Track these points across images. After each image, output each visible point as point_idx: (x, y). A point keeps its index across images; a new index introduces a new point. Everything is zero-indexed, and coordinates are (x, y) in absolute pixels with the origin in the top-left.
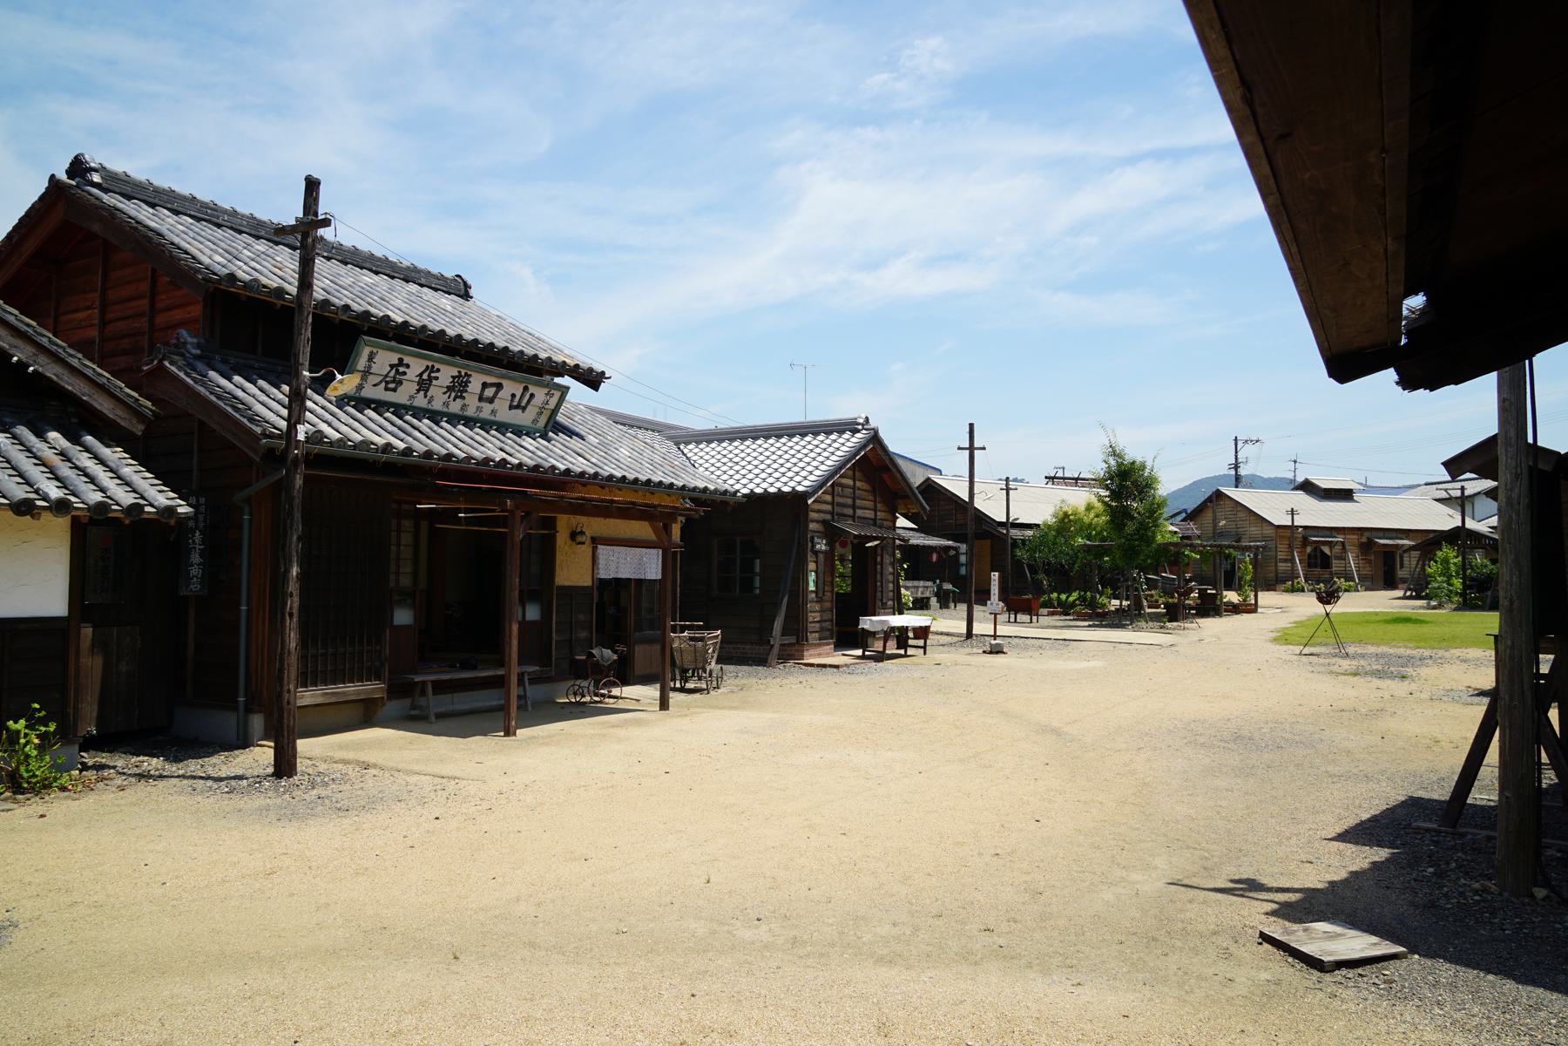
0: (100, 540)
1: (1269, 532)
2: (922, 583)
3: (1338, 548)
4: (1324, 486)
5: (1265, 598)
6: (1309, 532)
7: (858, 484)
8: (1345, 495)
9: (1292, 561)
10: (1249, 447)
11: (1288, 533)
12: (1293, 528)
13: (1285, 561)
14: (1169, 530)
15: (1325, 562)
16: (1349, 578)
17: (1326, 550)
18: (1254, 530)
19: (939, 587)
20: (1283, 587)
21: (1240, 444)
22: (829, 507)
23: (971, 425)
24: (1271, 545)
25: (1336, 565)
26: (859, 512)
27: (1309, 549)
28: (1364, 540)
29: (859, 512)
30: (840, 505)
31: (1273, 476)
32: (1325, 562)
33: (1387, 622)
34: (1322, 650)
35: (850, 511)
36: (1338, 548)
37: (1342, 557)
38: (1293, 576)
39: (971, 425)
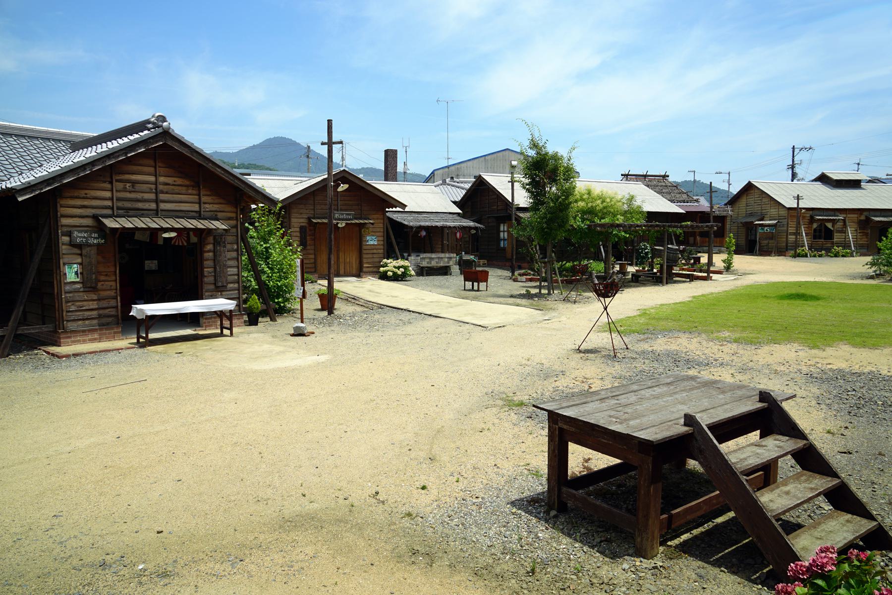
1: (783, 212)
2: (433, 256)
3: (839, 225)
4: (835, 177)
7: (162, 179)
8: (854, 184)
9: (800, 234)
12: (797, 209)
15: (829, 235)
16: (846, 245)
17: (829, 225)
18: (773, 211)
19: (461, 258)
21: (796, 151)
22: (109, 203)
24: (785, 222)
25: (837, 237)
26: (163, 206)
27: (815, 225)
28: (863, 218)
29: (163, 206)
30: (119, 199)
31: (261, 141)
32: (829, 235)
33: (783, 297)
35: (153, 206)
36: (839, 225)
37: (843, 231)
38: (797, 245)
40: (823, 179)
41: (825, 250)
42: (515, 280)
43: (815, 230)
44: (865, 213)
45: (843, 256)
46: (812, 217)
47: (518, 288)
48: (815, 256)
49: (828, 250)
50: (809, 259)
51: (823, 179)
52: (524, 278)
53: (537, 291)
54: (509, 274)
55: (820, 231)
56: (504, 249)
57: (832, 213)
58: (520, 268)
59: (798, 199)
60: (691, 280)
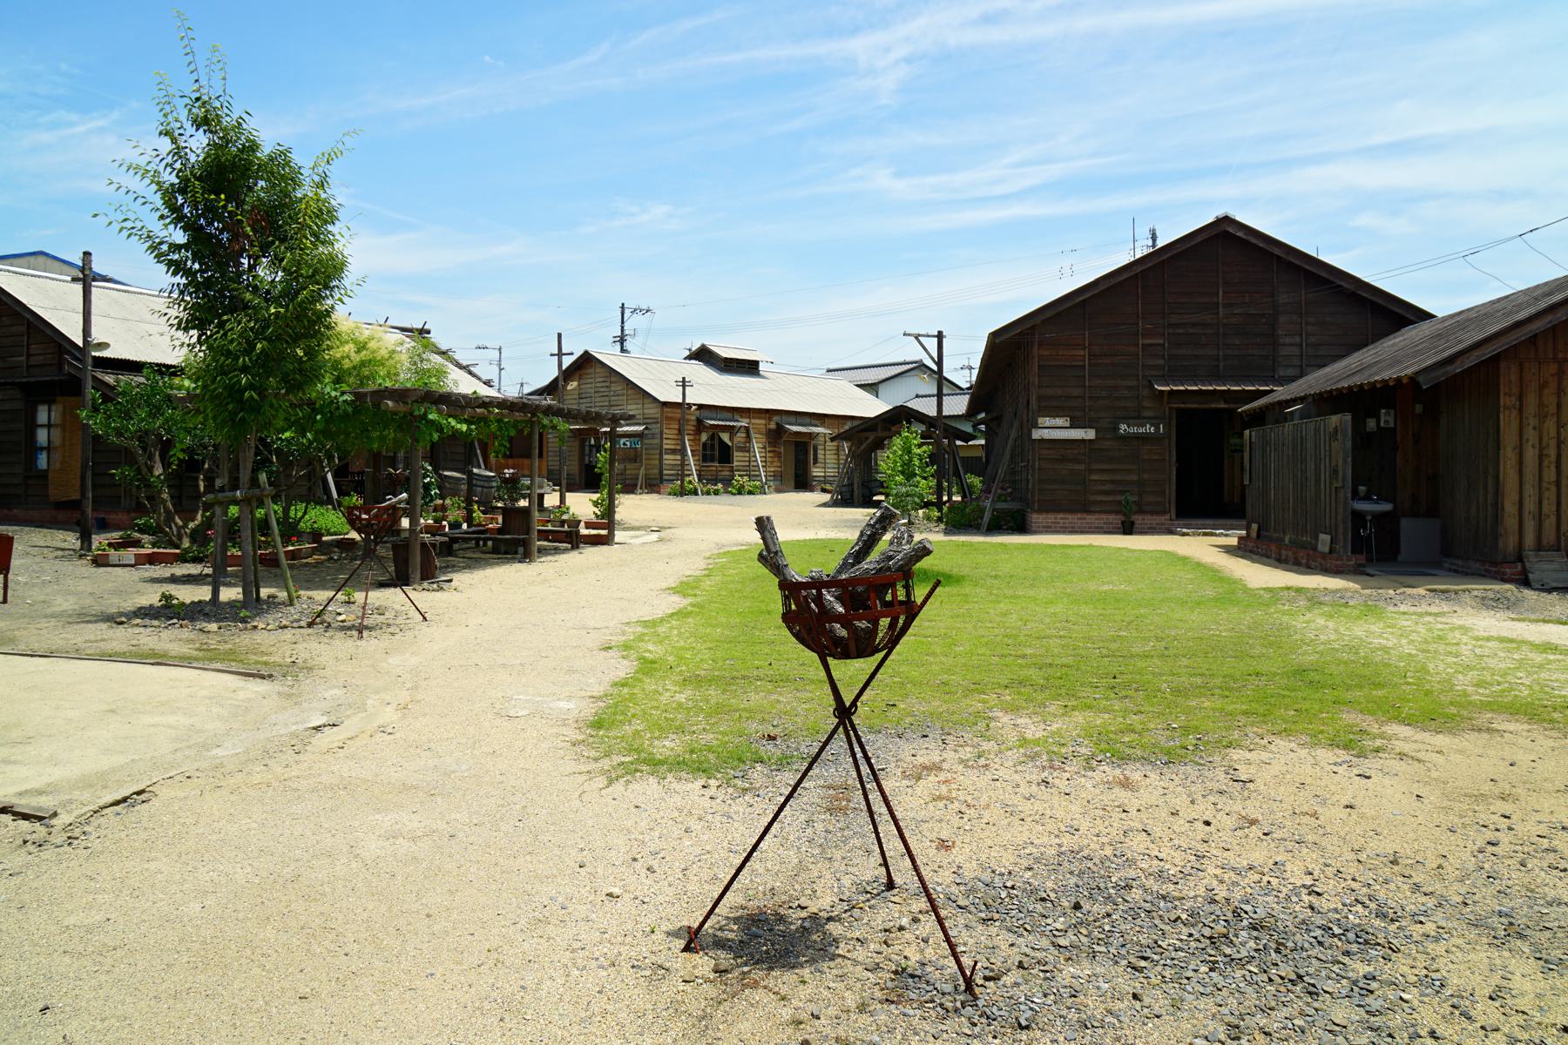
0: (1240, 538)
1: (652, 411)
3: (741, 435)
5: (629, 507)
6: (705, 413)
8: (749, 368)
9: (683, 452)
10: (638, 317)
11: (677, 413)
13: (673, 452)
14: (326, 388)
17: (725, 437)
20: (669, 487)
23: (560, 336)
24: (655, 428)
27: (704, 437)
28: (773, 426)
32: (725, 454)
34: (194, 569)
36: (741, 435)
37: (746, 449)
38: (682, 474)
39: (560, 336)
40: (703, 355)
41: (722, 481)
42: (100, 562)
43: (704, 445)
44: (776, 418)
45: (750, 493)
46: (699, 421)
47: (136, 585)
48: (708, 493)
49: (727, 482)
50: (700, 497)
51: (703, 355)
52: (129, 554)
53: (203, 593)
54: (71, 540)
55: (712, 446)
56: (44, 475)
57: (729, 415)
58: (103, 526)
59: (684, 386)
60: (575, 547)
